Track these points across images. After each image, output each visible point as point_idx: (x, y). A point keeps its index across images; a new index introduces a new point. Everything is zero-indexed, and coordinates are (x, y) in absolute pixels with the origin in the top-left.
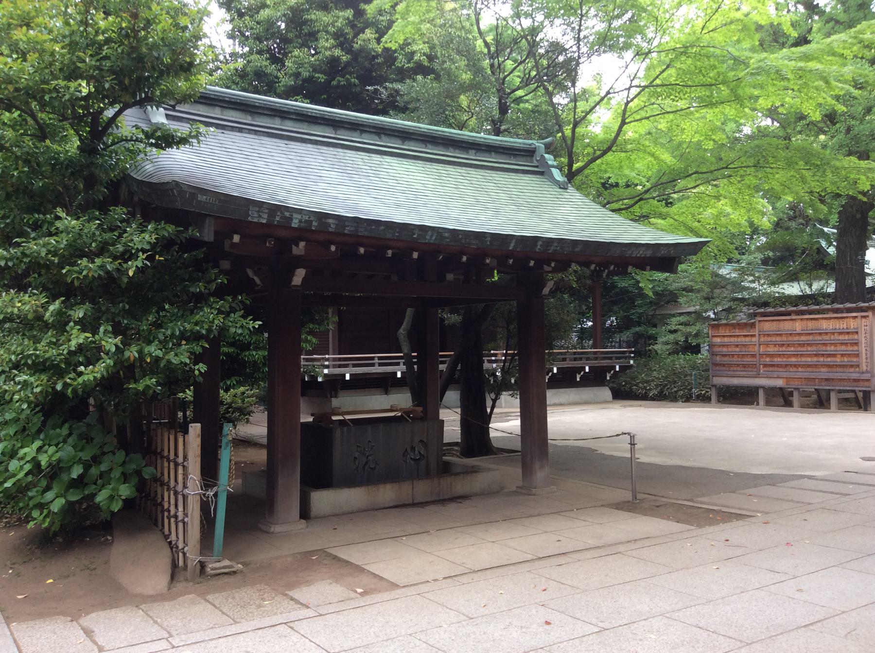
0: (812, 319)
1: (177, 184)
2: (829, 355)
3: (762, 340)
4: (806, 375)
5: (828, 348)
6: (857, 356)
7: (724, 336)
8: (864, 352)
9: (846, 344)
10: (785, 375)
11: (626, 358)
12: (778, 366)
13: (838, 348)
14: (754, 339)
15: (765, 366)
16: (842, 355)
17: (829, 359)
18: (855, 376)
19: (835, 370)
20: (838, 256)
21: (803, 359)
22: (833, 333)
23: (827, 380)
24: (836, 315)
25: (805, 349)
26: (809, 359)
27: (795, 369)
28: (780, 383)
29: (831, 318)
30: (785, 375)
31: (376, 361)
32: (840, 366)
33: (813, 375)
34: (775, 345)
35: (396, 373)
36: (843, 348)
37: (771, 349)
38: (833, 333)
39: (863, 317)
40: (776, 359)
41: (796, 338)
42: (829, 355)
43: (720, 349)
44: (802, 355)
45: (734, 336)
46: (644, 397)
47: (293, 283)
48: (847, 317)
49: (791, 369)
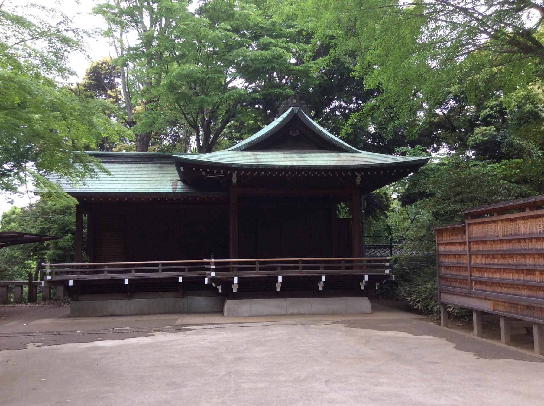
11: (379, 267)
15: (477, 282)
20: (367, 132)
24: (535, 213)
29: (488, 222)
31: (160, 267)
35: (123, 280)
37: (479, 261)
38: (531, 239)
46: (409, 309)
47: (180, 188)
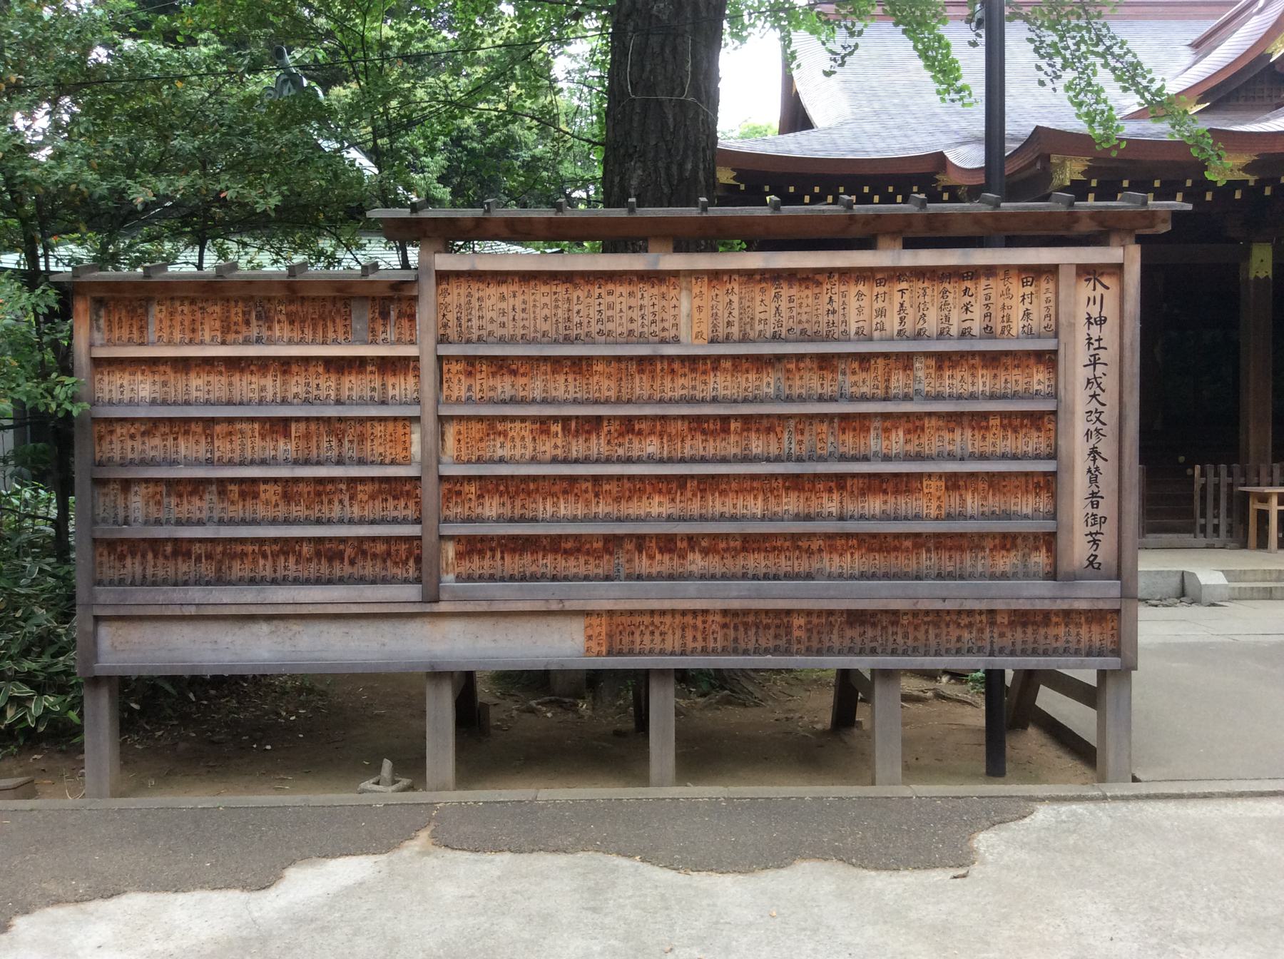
0: (920, 273)
1: (407, 674)
2: (876, 483)
3: (458, 387)
4: (736, 595)
5: (874, 443)
6: (1048, 483)
7: (183, 365)
8: (1081, 463)
9: (979, 420)
10: (607, 596)
12: (555, 545)
13: (933, 441)
14: (401, 386)
16: (954, 482)
17: (875, 504)
18: (1036, 593)
19: (981, 563)
21: (716, 505)
22: (906, 360)
23: (857, 618)
25: (731, 446)
26: (756, 506)
27: (664, 563)
28: (562, 645)
30: (607, 596)
32: (941, 542)
33: (778, 595)
34: (543, 423)
36: (963, 440)
37: (517, 455)
39: (1088, 272)
40: (545, 508)
41: (679, 386)
42: (876, 483)
43: (154, 446)
44: (708, 484)
45: (263, 364)
48: (989, 271)
49: (643, 564)
